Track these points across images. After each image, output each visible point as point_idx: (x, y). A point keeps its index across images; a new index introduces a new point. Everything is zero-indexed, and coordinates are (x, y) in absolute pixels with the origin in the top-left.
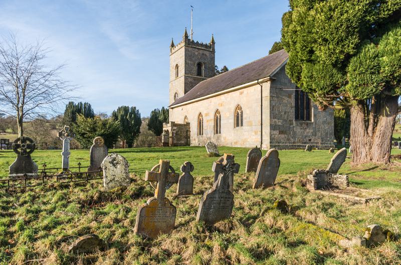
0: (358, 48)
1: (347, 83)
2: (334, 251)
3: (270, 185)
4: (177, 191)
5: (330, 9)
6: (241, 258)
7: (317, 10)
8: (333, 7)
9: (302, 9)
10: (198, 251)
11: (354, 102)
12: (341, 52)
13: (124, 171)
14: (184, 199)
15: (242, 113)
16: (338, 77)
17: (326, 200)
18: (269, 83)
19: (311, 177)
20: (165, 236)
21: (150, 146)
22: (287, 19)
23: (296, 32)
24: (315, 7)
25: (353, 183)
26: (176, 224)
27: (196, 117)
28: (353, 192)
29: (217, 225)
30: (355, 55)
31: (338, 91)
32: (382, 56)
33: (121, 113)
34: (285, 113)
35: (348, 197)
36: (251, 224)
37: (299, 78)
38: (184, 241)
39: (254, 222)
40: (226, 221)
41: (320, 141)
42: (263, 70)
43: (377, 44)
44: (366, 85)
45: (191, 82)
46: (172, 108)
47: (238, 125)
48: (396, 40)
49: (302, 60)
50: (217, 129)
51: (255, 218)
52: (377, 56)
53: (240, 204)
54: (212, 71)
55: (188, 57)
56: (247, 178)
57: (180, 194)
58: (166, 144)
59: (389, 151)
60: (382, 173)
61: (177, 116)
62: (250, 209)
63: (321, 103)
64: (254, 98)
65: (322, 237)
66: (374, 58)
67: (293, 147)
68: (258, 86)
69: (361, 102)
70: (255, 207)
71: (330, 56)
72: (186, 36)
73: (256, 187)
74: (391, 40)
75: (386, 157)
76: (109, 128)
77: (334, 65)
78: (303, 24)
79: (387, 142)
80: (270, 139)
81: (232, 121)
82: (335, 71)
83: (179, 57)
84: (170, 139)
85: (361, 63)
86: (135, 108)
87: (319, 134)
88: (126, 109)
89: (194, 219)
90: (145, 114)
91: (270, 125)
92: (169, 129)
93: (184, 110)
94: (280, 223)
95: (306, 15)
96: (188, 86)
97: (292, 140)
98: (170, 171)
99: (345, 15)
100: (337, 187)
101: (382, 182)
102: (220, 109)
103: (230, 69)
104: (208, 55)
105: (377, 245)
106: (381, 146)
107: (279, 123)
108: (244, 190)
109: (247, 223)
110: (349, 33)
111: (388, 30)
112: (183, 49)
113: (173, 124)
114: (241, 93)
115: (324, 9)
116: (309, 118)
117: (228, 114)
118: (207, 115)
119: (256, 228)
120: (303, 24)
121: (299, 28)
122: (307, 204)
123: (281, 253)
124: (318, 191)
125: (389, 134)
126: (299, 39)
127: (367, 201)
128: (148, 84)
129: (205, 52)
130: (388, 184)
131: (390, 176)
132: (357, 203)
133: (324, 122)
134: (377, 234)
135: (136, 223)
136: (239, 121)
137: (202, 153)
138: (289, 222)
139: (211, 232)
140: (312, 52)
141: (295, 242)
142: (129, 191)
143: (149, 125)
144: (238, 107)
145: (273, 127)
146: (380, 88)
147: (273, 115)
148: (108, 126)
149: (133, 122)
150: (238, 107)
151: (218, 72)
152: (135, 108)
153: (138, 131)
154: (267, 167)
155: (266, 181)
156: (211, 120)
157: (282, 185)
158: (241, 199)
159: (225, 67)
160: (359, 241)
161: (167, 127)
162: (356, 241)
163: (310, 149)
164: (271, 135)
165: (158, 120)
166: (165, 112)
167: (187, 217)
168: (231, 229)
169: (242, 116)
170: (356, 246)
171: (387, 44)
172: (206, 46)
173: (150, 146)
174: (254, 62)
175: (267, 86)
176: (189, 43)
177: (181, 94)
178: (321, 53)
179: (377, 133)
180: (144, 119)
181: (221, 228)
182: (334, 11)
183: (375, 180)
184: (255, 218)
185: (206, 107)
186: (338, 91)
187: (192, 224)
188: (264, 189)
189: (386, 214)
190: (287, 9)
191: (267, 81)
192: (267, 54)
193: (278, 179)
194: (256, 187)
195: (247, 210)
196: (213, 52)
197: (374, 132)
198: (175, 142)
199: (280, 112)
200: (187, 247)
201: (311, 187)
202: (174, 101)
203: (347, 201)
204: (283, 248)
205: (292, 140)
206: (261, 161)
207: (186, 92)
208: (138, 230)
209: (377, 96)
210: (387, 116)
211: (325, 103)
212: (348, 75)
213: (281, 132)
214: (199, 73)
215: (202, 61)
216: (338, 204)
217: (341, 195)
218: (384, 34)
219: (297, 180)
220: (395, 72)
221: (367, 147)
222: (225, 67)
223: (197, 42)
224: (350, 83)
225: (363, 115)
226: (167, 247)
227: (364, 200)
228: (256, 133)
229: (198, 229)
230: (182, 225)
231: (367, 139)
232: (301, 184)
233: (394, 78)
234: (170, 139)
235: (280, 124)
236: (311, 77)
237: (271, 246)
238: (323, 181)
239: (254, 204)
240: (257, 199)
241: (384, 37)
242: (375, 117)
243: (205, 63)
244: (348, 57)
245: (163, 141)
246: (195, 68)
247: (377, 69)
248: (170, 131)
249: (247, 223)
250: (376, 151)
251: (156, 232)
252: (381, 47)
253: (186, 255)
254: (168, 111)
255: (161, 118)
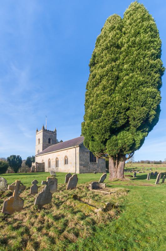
0: (110, 136)
1: (106, 149)
2: (91, 214)
3: (74, 188)
4: (30, 192)
5: (99, 123)
6: (49, 220)
7: (94, 122)
8: (100, 122)
9: (89, 121)
10: (31, 218)
11: (110, 156)
12: (104, 138)
13: (4, 184)
14: (33, 195)
15: (68, 159)
16: (103, 147)
17: (96, 193)
18: (79, 147)
19: (90, 185)
20: (17, 213)
21: (26, 172)
22: (83, 125)
23: (86, 129)
24: (93, 121)
25: (108, 186)
26: (23, 208)
27: (48, 160)
28: (107, 190)
29: (44, 206)
30: (109, 139)
31: (104, 152)
32: (119, 140)
33: (12, 158)
34: (86, 159)
35: (104, 192)
36: (60, 205)
37: (88, 147)
38: (25, 214)
39: (62, 204)
40: (48, 204)
41: (100, 170)
42: (76, 142)
43: (116, 136)
44: (113, 150)
45: (45, 146)
46: (37, 156)
47: (66, 164)
48: (123, 135)
49: (89, 140)
50: (57, 165)
51: (62, 202)
52: (117, 140)
53: (58, 197)
54: (55, 142)
55: (44, 136)
56: (65, 185)
57: (31, 193)
58: (33, 171)
59: (123, 174)
60: (120, 182)
61: (39, 160)
62: (62, 199)
63: (97, 156)
64: (73, 153)
65: (88, 209)
66: (116, 141)
67: (89, 172)
68: (74, 149)
69: (112, 156)
70: (64, 198)
71: (100, 139)
72: (44, 128)
73: (68, 189)
74: (122, 135)
75: (122, 176)
76: (3, 165)
77: (102, 142)
78: (89, 127)
79: (122, 171)
80: (80, 169)
81: (63, 162)
82: (102, 145)
83: (40, 135)
84: (35, 169)
85: (111, 142)
86: (19, 156)
87: (100, 167)
88: (14, 156)
89: (34, 204)
90: (24, 158)
91: (80, 164)
92: (35, 165)
93: (42, 157)
94: (73, 204)
95: (90, 123)
96: (44, 148)
97: (89, 170)
98: (21, 185)
99: (104, 125)
100: (102, 188)
101: (120, 186)
102: (58, 157)
103: (64, 141)
104: (53, 136)
105: (108, 210)
106: (120, 172)
107: (83, 163)
108: (62, 191)
109: (58, 205)
110: (106, 132)
111: (121, 131)
112: (42, 133)
113: (37, 163)
114: (67, 151)
115: (96, 122)
116: (95, 161)
117: (61, 159)
118: (52, 159)
119: (61, 207)
120: (89, 127)
121: (87, 128)
122: (87, 195)
123: (69, 216)
124: (93, 190)
125: (123, 168)
126: (88, 132)
127: (110, 193)
128: (29, 147)
129: (53, 134)
130: (121, 186)
131: (123, 183)
132: (107, 194)
133: (102, 163)
134: (109, 206)
135: (3, 208)
136: (66, 162)
137: (49, 175)
138: (76, 203)
139: (41, 209)
140: (93, 137)
141: (77, 211)
142: (6, 193)
143: (26, 163)
144: (66, 157)
145: (80, 165)
146: (118, 151)
147: (80, 160)
148: (2, 164)
149: (18, 162)
150: (66, 157)
151: (58, 142)
152: (19, 156)
153: (21, 166)
154: (73, 180)
155: (72, 187)
156: (54, 162)
157: (79, 188)
158: (55, 195)
159: (61, 140)
160: (101, 209)
161: (34, 164)
162: (100, 210)
163: (96, 173)
164: (80, 168)
165: (30, 161)
166: (34, 158)
167: (30, 204)
168: (51, 208)
169: (67, 160)
170: (100, 211)
171: (120, 136)
172: (53, 132)
173: (26, 172)
174: (73, 139)
175: (78, 149)
176: (45, 130)
177: (41, 151)
178: (97, 138)
179: (119, 167)
180: (24, 160)
181: (46, 208)
182: (100, 123)
183: (117, 185)
184: (62, 202)
185: (52, 156)
186: (104, 152)
187: (32, 207)
188: (71, 190)
189: (117, 198)
190: (83, 121)
191: (78, 147)
192: (80, 136)
193: (78, 185)
194: (68, 189)
195: (60, 199)
196: (56, 134)
197: (117, 167)
198: (37, 170)
199: (83, 159)
200: (26, 217)
201: (90, 188)
202: (37, 153)
203: (103, 193)
204: (71, 214)
205: (89, 170)
206: (70, 179)
207: (43, 150)
208: (3, 211)
209: (118, 154)
210: (123, 161)
211: (99, 156)
212: (107, 146)
213: (84, 167)
214: (49, 142)
215: (51, 138)
216: (100, 195)
217: (101, 191)
218: (119, 132)
219: (85, 186)
220: (123, 146)
221: (115, 173)
222: (61, 140)
223: (47, 130)
224: (108, 149)
225: (113, 161)
226: (17, 218)
227: (109, 193)
228: (73, 167)
229: (34, 209)
230: (27, 207)
231: (115, 170)
232: (86, 188)
233: (123, 148)
234: (35, 169)
235: (83, 163)
236: (93, 146)
237: (65, 214)
238: (96, 186)
239: (64, 196)
240: (66, 194)
241: (119, 133)
242: (118, 162)
243: (52, 139)
244: (106, 140)
245: (31, 170)
246: (48, 140)
247: (116, 145)
248: (35, 166)
249: (58, 205)
250: (118, 174)
251: (13, 211)
252: (118, 137)
253: (24, 221)
254: (35, 157)
255: (32, 160)
